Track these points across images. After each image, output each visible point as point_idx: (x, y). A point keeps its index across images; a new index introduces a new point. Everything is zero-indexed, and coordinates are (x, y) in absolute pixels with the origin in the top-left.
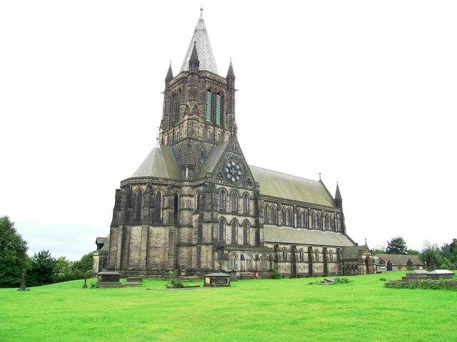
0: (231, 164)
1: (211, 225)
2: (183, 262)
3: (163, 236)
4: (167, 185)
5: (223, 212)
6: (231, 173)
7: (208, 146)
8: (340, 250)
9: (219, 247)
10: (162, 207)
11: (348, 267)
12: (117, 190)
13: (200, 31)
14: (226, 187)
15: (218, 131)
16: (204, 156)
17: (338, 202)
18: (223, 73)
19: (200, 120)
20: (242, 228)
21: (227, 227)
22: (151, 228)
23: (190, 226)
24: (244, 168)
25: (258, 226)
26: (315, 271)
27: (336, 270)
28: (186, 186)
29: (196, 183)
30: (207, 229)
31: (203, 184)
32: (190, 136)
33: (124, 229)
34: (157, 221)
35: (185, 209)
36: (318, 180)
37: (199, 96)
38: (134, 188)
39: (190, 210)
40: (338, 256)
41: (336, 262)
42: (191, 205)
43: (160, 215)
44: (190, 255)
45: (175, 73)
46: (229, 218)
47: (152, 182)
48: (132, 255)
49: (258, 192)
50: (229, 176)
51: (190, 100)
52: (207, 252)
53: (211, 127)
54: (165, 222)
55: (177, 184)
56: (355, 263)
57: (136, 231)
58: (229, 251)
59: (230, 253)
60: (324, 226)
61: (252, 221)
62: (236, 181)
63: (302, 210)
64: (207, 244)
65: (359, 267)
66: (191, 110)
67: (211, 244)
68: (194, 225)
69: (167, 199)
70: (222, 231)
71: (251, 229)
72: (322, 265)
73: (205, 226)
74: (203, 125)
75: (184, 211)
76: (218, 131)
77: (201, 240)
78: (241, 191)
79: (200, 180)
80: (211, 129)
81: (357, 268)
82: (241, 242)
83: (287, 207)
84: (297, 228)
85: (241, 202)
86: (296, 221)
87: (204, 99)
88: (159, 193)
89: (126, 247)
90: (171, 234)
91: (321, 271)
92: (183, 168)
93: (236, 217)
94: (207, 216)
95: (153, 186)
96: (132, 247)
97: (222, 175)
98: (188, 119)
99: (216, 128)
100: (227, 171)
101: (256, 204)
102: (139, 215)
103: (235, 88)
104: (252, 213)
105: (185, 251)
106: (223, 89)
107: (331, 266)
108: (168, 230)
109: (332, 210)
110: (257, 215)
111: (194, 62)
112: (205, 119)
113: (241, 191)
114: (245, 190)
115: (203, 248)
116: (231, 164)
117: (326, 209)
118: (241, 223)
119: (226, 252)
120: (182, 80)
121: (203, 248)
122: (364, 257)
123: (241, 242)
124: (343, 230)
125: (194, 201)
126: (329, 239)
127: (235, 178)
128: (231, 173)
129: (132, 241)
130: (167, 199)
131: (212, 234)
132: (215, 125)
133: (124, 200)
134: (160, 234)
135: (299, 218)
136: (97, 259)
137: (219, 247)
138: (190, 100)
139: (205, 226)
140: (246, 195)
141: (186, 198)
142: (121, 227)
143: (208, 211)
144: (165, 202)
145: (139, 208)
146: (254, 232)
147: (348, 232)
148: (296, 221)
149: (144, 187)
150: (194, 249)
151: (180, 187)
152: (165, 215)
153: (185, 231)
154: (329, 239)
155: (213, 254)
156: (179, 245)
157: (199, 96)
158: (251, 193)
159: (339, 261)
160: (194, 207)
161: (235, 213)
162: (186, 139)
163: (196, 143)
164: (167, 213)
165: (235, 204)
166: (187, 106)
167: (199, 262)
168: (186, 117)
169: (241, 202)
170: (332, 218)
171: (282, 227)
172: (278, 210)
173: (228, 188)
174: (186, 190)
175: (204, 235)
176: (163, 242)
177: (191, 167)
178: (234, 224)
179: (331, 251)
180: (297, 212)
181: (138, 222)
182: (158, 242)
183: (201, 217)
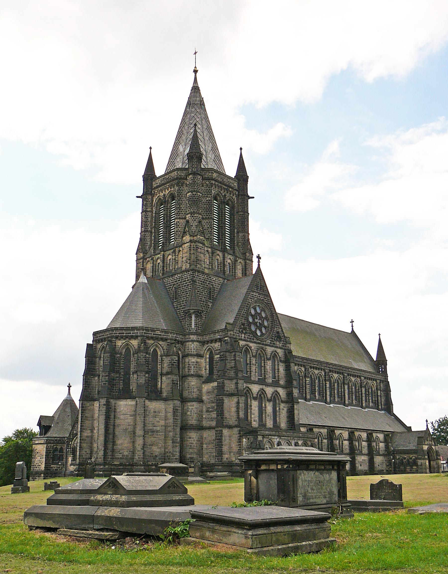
0: (255, 310)
1: (235, 399)
2: (190, 453)
3: (162, 414)
4: (166, 340)
5: (248, 380)
6: (255, 324)
7: (217, 281)
8: (389, 437)
9: (246, 430)
10: (159, 371)
11: (402, 463)
12: (88, 345)
13: (196, 102)
14: (251, 344)
15: (229, 259)
16: (212, 295)
17: (381, 362)
18: (231, 171)
19: (206, 242)
20: (271, 403)
21: (253, 402)
22: (147, 402)
23: (200, 400)
24: (272, 316)
25: (291, 401)
26: (359, 467)
27: (385, 466)
28: (193, 341)
29: (207, 338)
30: (230, 404)
31: (220, 340)
32: (193, 267)
33: (108, 404)
34: (154, 394)
35: (192, 375)
36: (349, 331)
37: (196, 207)
38: (119, 343)
39: (199, 376)
40: (387, 447)
41: (383, 455)
42: (200, 369)
43: (156, 384)
44: (201, 441)
45: (160, 170)
46: (255, 388)
47: (146, 335)
48: (119, 442)
49: (290, 352)
50: (253, 328)
51: (191, 213)
52: (230, 437)
53: (221, 254)
54: (165, 395)
55: (179, 338)
56: (413, 456)
57: (125, 406)
58: (263, 436)
59: (265, 440)
60: (364, 402)
61: (282, 392)
62: (262, 334)
63: (336, 376)
64: (230, 427)
65: (419, 462)
66: (194, 228)
67: (236, 426)
68: (204, 398)
69: (167, 360)
70: (247, 407)
71: (282, 405)
72: (365, 458)
73: (226, 400)
74: (209, 249)
75: (190, 378)
76: (229, 259)
77: (221, 422)
78: (269, 350)
79: (214, 333)
80: (219, 256)
81: (415, 463)
82: (270, 423)
83: (317, 372)
84: (330, 403)
85: (269, 364)
86: (328, 393)
87: (209, 210)
88: (155, 351)
89: (111, 431)
90: (175, 411)
91: (365, 467)
92: (188, 314)
93: (264, 387)
94: (230, 386)
95: (148, 341)
96: (118, 431)
97: (245, 328)
98: (191, 241)
99: (226, 255)
100: (251, 320)
101: (288, 369)
102: (127, 382)
103: (250, 194)
104: (282, 382)
105: (193, 436)
106: (234, 194)
107: (378, 460)
108: (171, 406)
109: (374, 376)
110: (289, 385)
111: (195, 155)
112: (212, 241)
113: (269, 350)
114: (273, 349)
115: (226, 432)
116: (255, 310)
117: (367, 375)
118: (269, 396)
119: (260, 438)
120: (175, 177)
121: (226, 432)
122: (425, 447)
123: (270, 423)
124: (388, 407)
125: (204, 363)
126: (364, 419)
127: (261, 331)
128: (255, 324)
129: (117, 422)
130: (167, 360)
131: (238, 412)
132: (224, 250)
133: (101, 363)
134: (160, 411)
135: (332, 388)
136: (40, 449)
137: (246, 430)
138: (191, 213)
139: (226, 400)
140: (274, 355)
141: (194, 360)
142: (103, 401)
143: (231, 379)
144: (165, 364)
145: (127, 373)
146: (285, 409)
147: (396, 411)
148: (328, 393)
149: (135, 343)
150: (209, 435)
151: (182, 343)
152: (164, 384)
153: (193, 408)
154: (364, 419)
155: (240, 441)
156: (184, 428)
157: (196, 207)
158: (280, 352)
159: (388, 453)
160: (205, 372)
161: (262, 381)
162: (187, 271)
163: (202, 277)
164: (169, 381)
165: (262, 368)
166: (188, 222)
167: (220, 453)
168: (187, 238)
169: (269, 364)
170: (374, 389)
171: (311, 403)
172: (305, 376)
173: (253, 346)
174: (192, 347)
175: (226, 414)
176: (162, 423)
177: (198, 314)
178: (261, 397)
179: (377, 438)
180: (330, 378)
181: (126, 394)
182: (156, 424)
183: (221, 388)
